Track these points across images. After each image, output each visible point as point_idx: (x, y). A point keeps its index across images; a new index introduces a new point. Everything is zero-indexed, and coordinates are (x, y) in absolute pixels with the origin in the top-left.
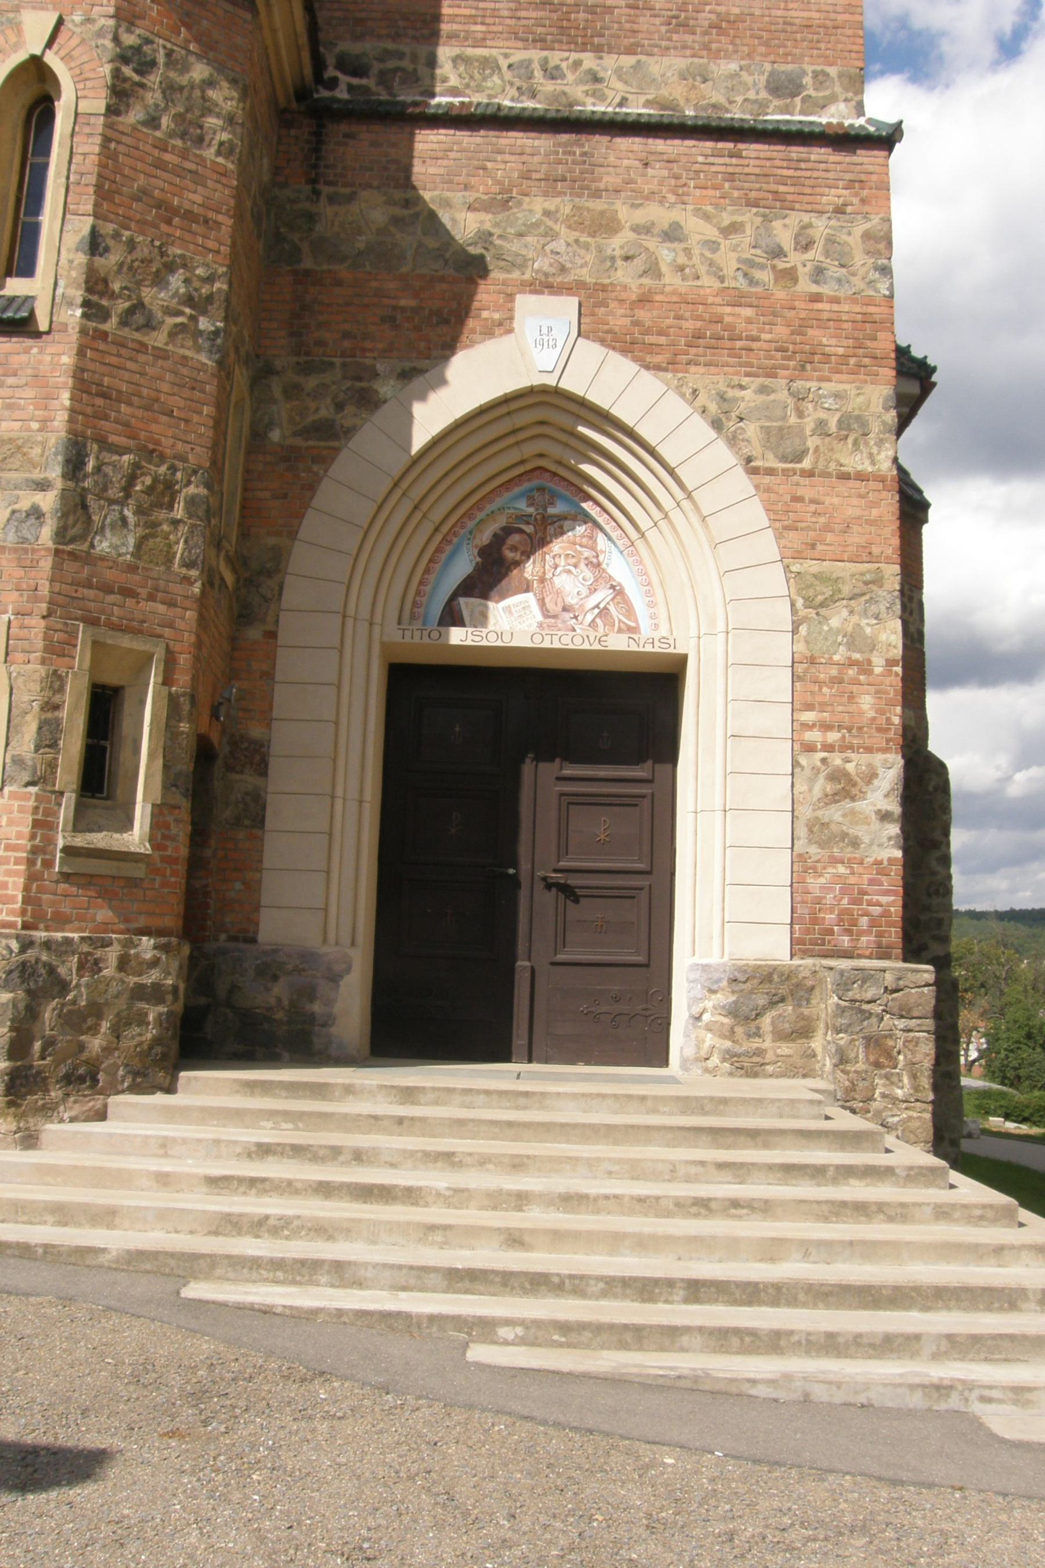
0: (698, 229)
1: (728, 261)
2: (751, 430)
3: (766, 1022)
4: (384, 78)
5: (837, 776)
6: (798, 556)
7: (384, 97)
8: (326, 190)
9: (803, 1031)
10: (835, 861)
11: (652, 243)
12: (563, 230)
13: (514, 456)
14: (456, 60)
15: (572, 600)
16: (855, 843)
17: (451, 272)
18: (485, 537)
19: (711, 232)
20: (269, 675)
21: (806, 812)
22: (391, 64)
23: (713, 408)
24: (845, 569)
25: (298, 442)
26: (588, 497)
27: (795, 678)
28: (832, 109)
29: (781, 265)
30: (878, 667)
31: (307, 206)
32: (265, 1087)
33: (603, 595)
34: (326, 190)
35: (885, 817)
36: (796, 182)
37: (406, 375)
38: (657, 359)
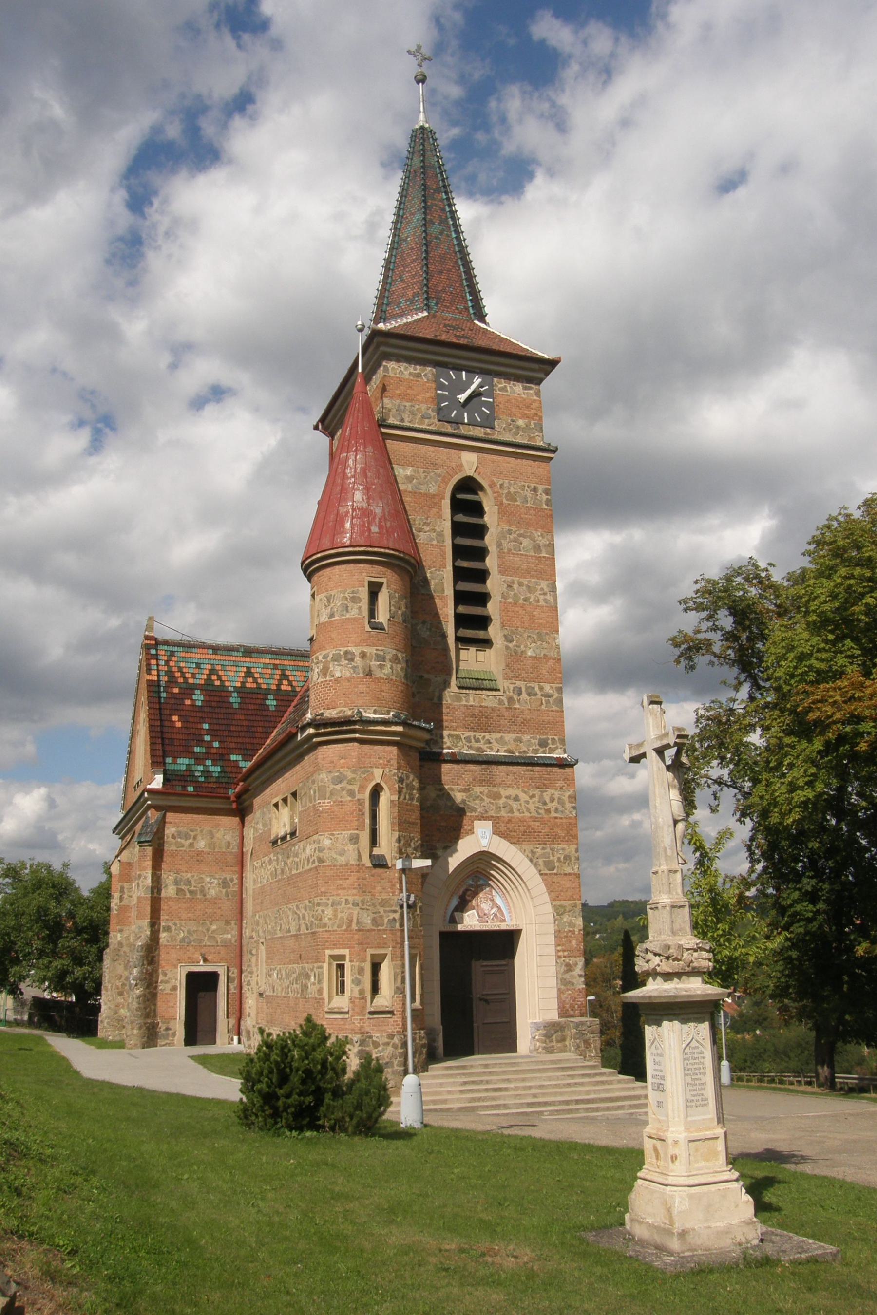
0: (523, 797)
1: (532, 807)
2: (541, 861)
6: (554, 900)
7: (428, 749)
9: (563, 1039)
10: (568, 990)
11: (510, 802)
12: (486, 798)
14: (449, 736)
15: (486, 912)
16: (573, 984)
17: (455, 813)
18: (461, 892)
19: (527, 798)
21: (560, 976)
23: (530, 855)
26: (491, 880)
27: (556, 937)
28: (557, 751)
29: (546, 808)
32: (450, 1068)
33: (494, 910)
35: (580, 976)
37: (446, 848)
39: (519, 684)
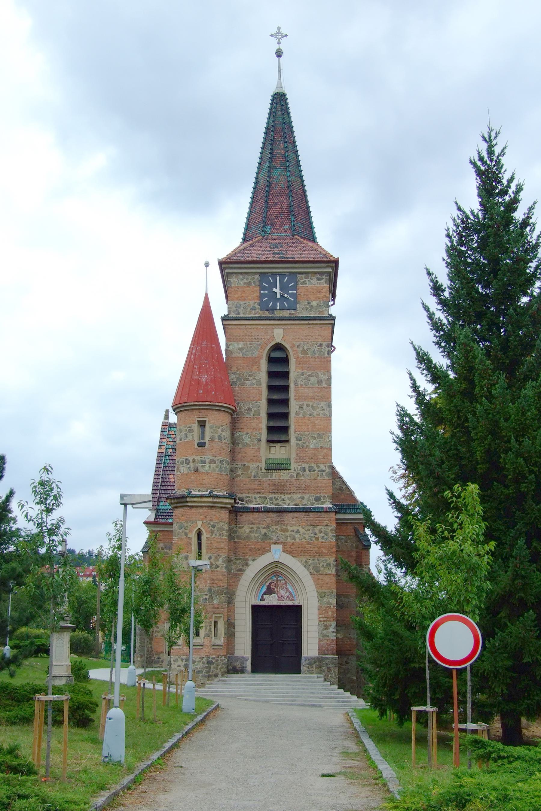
0: (302, 531)
1: (307, 536)
2: (311, 567)
3: (314, 665)
4: (247, 502)
5: (325, 626)
6: (319, 589)
8: (238, 526)
10: (325, 639)
11: (294, 534)
13: (272, 571)
15: (283, 595)
18: (268, 584)
20: (234, 612)
21: (320, 632)
22: (248, 499)
23: (304, 564)
24: (326, 591)
25: (236, 572)
27: (318, 609)
30: (332, 607)
31: (235, 529)
33: (288, 594)
34: (238, 526)
36: (319, 520)
38: (295, 555)
39: (303, 465)
